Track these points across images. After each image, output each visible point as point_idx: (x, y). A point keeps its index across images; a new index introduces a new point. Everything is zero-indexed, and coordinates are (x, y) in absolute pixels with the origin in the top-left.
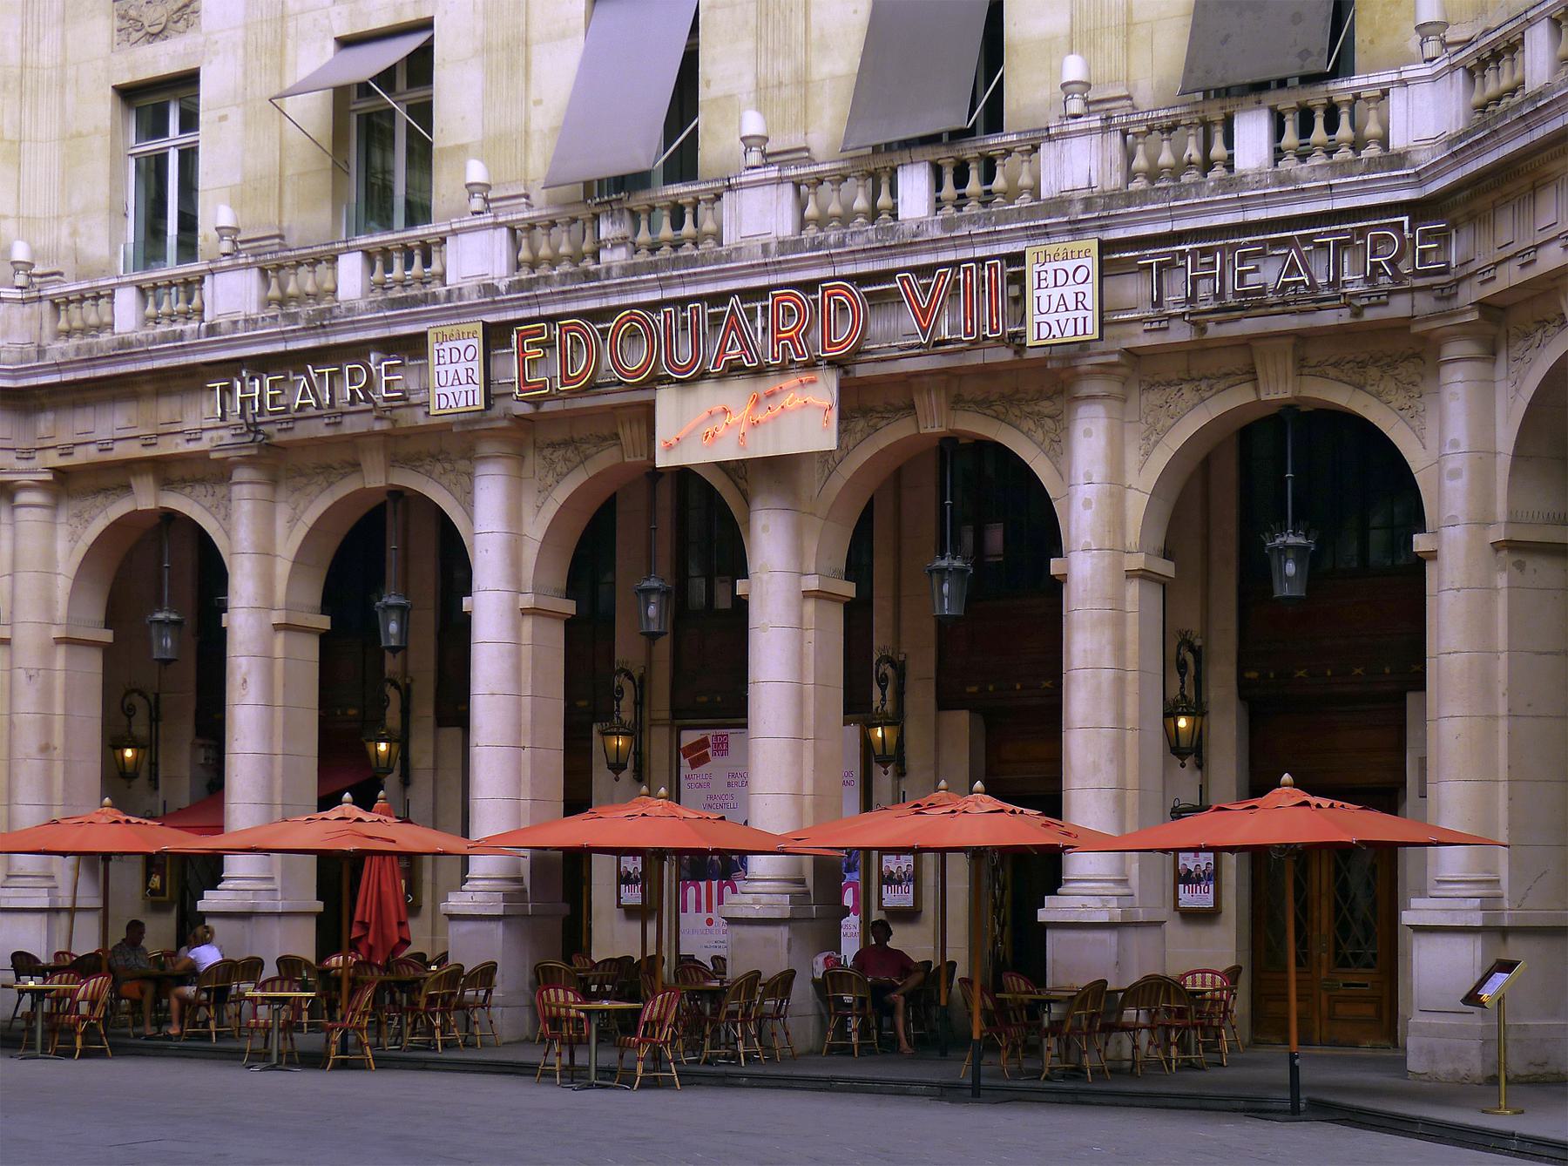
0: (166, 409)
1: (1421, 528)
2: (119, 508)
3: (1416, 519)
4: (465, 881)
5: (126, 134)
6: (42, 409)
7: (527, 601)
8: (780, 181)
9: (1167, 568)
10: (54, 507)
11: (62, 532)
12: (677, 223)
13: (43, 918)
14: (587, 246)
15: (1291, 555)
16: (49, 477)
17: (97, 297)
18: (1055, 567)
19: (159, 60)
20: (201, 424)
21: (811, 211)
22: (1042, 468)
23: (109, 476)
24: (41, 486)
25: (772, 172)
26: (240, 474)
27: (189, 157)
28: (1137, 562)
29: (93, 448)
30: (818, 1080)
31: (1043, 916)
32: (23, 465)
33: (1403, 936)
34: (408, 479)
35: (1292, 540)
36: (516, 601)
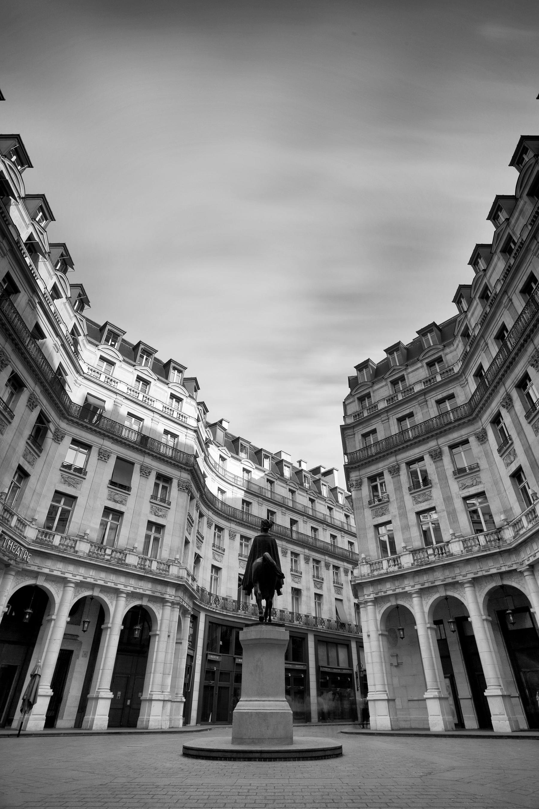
0: (379, 587)
1: (416, 625)
2: (388, 605)
3: (415, 624)
4: (427, 690)
5: (517, 485)
6: (406, 578)
7: (380, 632)
8: (459, 541)
9: (490, 618)
10: (375, 605)
11: (377, 611)
12: (394, 561)
13: (162, 703)
14: (426, 555)
15: (511, 615)
16: (528, 567)
17: (518, 523)
18: (416, 627)
19: (513, 468)
20: (409, 586)
21: (415, 558)
22: (462, 600)
23: (432, 589)
24: (371, 601)
25: (457, 539)
26: (526, 574)
27: (527, 483)
28: (429, 625)
29: (382, 593)
30: (409, 734)
31: (485, 694)
32: (412, 589)
33: (141, 701)
34: (400, 602)
35: (137, 627)
36: (481, 618)
